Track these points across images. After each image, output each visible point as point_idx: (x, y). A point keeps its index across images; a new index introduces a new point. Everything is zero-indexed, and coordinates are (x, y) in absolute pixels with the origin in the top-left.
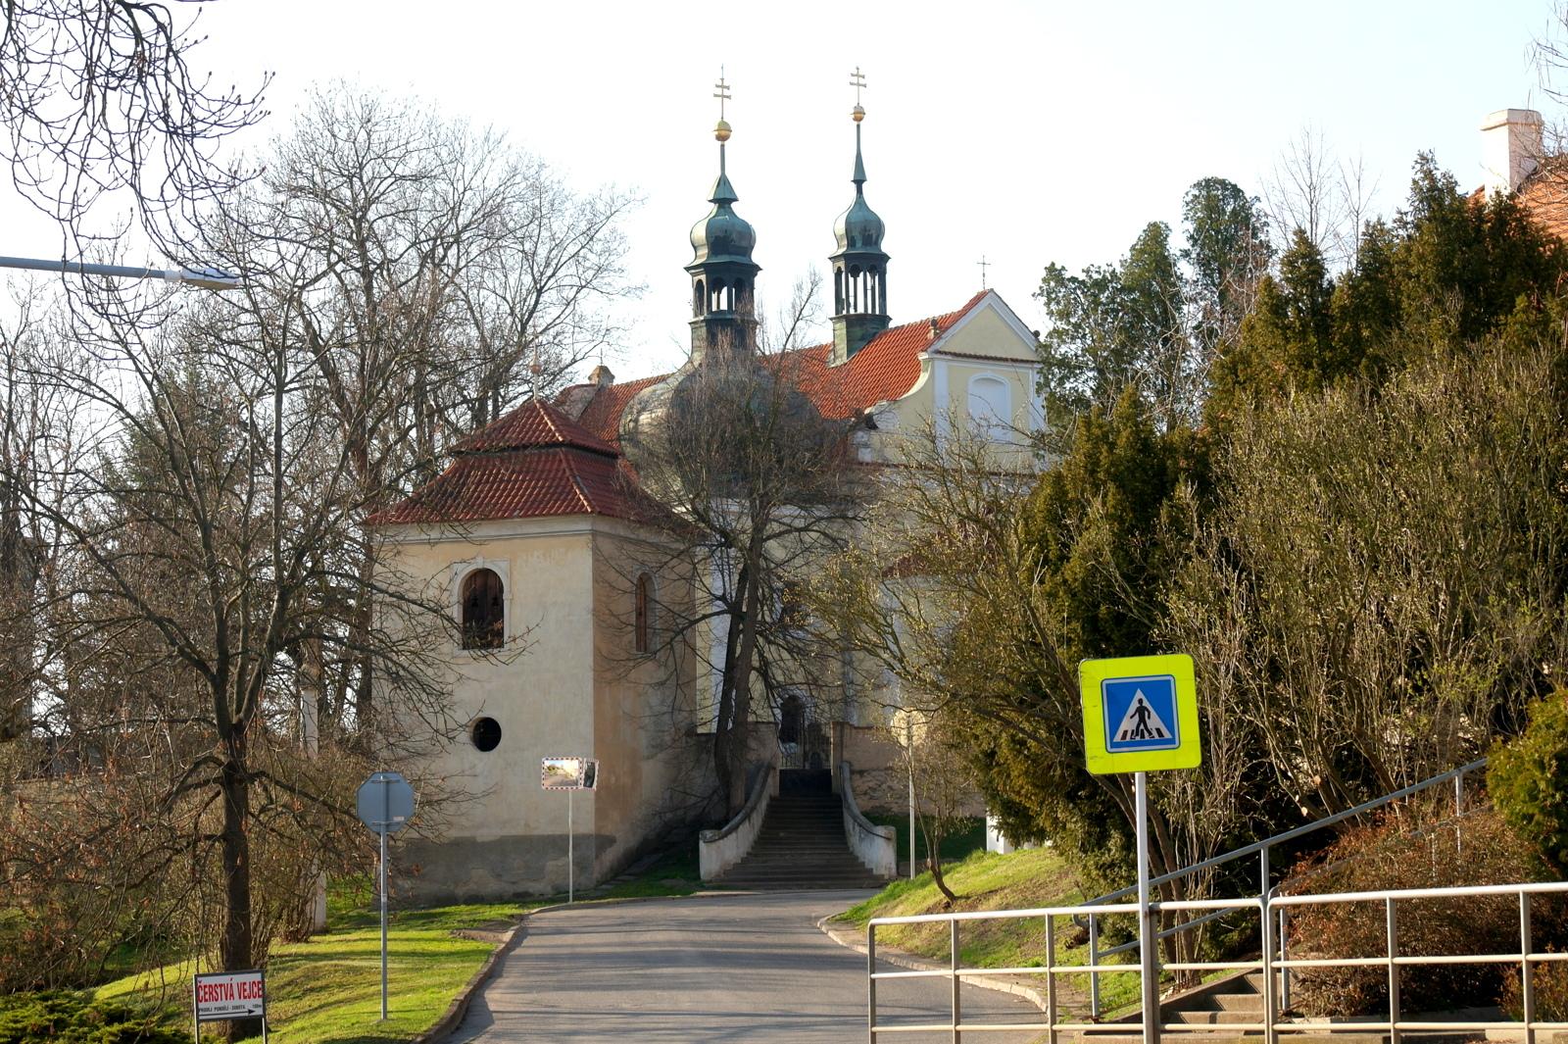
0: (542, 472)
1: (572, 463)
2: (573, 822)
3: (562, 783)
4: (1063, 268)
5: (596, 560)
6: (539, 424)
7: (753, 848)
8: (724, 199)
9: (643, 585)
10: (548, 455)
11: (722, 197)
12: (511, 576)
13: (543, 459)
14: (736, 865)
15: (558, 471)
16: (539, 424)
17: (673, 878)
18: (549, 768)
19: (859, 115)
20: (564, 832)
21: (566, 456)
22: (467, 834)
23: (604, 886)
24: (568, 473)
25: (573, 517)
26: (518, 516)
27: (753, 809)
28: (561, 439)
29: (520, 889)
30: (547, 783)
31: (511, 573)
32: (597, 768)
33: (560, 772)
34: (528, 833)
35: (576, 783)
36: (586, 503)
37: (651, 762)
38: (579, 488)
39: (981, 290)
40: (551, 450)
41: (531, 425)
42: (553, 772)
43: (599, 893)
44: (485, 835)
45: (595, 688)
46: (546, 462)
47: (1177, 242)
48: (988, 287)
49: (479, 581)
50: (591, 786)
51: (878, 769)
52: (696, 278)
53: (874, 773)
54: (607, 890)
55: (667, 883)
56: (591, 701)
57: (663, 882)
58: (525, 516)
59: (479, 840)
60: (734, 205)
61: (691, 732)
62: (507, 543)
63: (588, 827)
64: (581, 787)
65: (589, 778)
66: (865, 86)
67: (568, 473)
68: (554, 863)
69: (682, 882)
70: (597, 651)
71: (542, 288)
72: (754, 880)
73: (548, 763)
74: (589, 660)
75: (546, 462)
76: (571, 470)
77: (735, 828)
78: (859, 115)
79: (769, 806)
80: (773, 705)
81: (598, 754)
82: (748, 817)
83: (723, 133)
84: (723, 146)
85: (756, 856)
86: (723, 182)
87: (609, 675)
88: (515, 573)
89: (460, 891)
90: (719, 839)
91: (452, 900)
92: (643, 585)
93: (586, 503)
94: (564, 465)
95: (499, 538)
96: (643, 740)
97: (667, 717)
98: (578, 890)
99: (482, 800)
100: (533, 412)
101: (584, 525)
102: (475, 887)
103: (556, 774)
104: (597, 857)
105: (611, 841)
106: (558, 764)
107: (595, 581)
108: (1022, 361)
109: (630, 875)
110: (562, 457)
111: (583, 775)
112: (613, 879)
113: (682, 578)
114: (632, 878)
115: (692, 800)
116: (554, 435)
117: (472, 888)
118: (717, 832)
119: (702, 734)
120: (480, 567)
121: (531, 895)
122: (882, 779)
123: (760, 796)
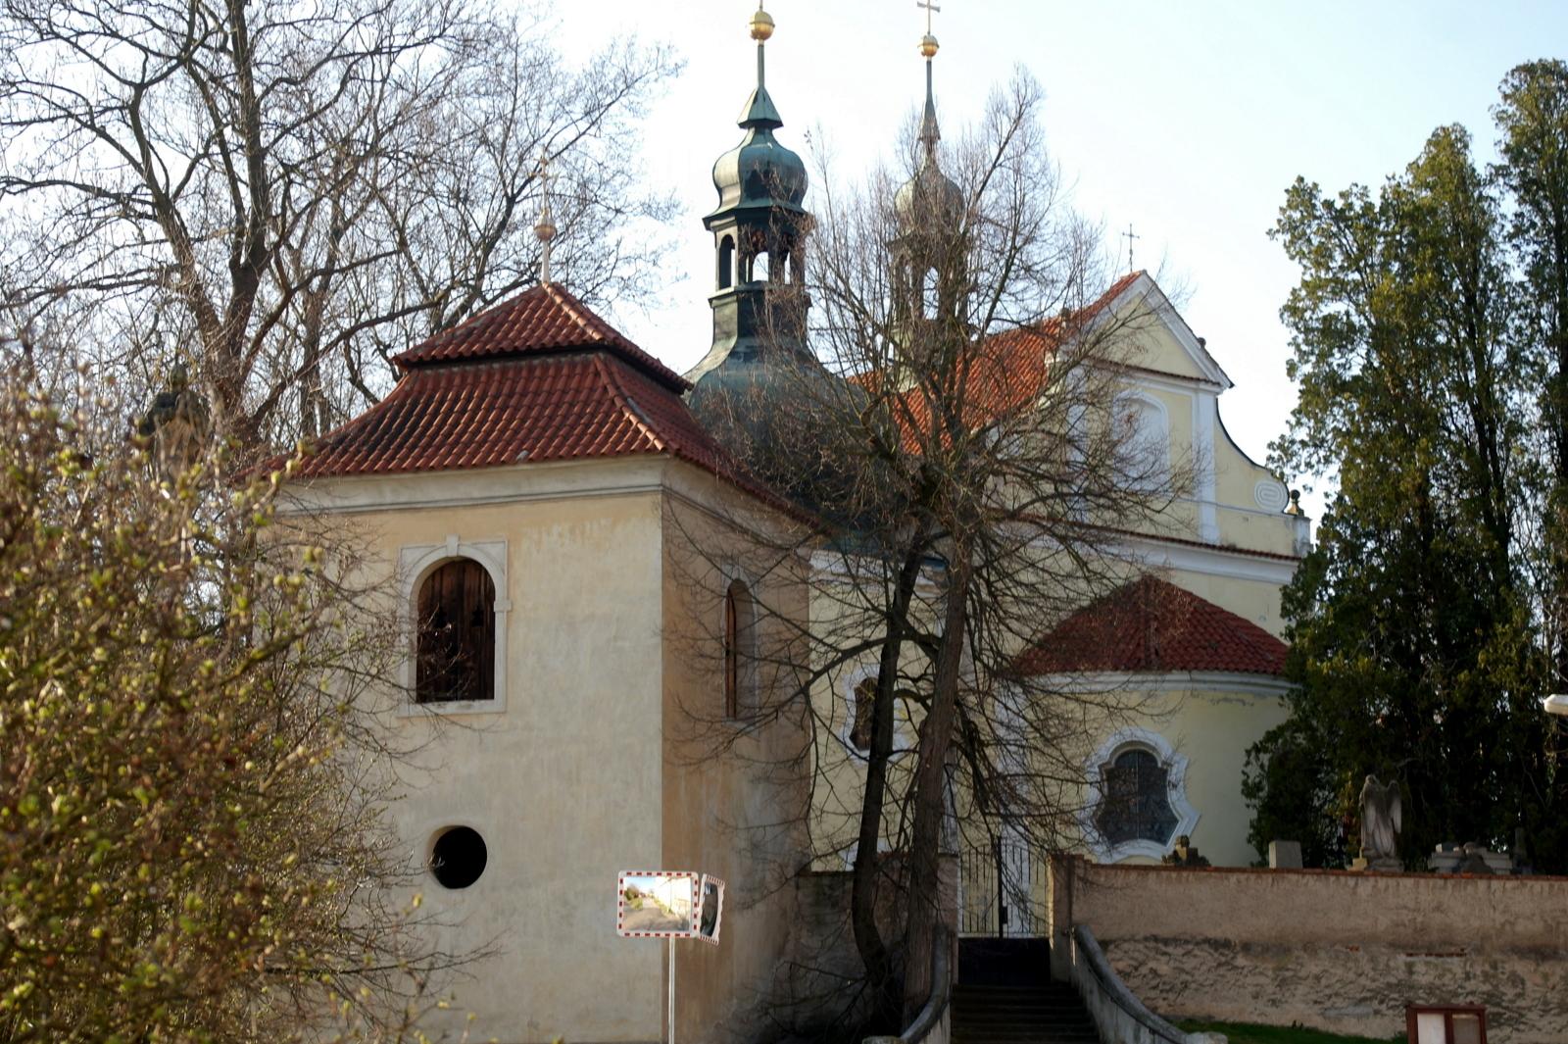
0: (564, 392)
3: (651, 926)
4: (1315, 185)
5: (667, 540)
6: (554, 319)
8: (763, 122)
10: (573, 366)
11: (761, 116)
12: (508, 568)
15: (592, 390)
16: (554, 319)
19: (930, 48)
24: (611, 392)
26: (531, 461)
28: (596, 336)
30: (628, 922)
33: (647, 903)
35: (684, 925)
36: (651, 437)
38: (634, 413)
39: (1126, 273)
42: (634, 903)
46: (569, 377)
47: (1485, 152)
48: (1136, 269)
49: (448, 582)
51: (1132, 939)
52: (721, 234)
53: (1126, 946)
56: (656, 796)
58: (542, 458)
60: (777, 133)
61: (803, 871)
66: (938, 10)
67: (611, 392)
71: (514, 196)
74: (655, 721)
75: (569, 377)
76: (618, 388)
78: (930, 48)
83: (763, 27)
84: (761, 47)
86: (761, 97)
88: (517, 564)
92: (736, 596)
93: (651, 437)
94: (604, 379)
95: (476, 504)
99: (470, 968)
100: (541, 300)
101: (648, 476)
103: (639, 908)
106: (643, 884)
107: (665, 576)
108: (1184, 378)
110: (600, 367)
116: (584, 332)
122: (1141, 958)
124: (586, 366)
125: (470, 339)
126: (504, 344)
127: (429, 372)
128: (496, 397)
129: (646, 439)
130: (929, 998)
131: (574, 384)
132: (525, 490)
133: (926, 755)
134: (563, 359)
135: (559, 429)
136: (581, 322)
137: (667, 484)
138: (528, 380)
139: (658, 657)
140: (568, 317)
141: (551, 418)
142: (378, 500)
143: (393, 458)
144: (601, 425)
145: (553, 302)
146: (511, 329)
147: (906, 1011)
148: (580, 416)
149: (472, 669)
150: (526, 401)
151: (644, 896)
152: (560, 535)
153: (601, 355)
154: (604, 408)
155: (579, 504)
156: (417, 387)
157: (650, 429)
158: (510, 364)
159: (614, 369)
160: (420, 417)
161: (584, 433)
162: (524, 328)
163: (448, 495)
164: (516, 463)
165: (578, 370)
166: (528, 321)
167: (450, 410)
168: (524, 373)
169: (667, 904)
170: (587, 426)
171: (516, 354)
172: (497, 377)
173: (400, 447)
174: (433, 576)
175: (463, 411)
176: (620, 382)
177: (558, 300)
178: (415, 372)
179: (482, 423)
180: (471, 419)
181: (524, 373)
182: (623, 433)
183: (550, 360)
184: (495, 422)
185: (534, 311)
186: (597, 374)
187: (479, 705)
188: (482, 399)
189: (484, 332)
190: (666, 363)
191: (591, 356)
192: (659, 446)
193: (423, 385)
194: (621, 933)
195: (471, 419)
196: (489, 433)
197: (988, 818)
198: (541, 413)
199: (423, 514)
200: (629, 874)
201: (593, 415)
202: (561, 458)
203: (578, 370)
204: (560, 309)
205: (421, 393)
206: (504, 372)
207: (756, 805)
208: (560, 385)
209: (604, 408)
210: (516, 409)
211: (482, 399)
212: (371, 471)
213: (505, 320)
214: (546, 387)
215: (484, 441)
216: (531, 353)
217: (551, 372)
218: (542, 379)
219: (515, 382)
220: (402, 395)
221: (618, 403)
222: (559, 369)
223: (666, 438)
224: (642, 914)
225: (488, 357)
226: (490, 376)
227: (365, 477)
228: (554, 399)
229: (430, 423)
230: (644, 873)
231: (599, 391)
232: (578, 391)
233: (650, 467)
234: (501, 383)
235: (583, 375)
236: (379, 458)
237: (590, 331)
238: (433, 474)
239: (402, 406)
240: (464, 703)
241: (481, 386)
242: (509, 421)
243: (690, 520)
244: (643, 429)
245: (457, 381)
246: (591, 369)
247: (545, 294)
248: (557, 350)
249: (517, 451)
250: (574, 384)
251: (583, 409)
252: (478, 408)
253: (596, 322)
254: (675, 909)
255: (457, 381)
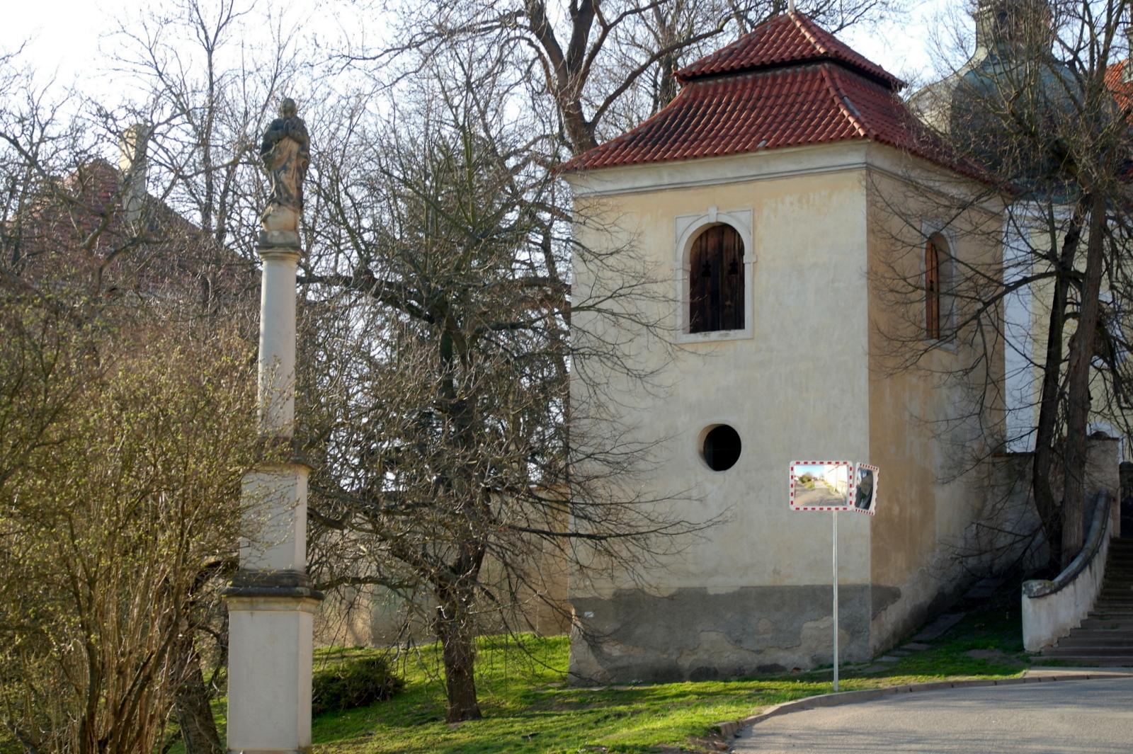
0: (798, 95)
1: (839, 84)
2: (840, 569)
3: (822, 502)
5: (871, 203)
6: (794, 39)
7: (1095, 606)
9: (935, 245)
10: (805, 74)
12: (753, 230)
13: (799, 79)
14: (1074, 630)
15: (818, 92)
16: (794, 39)
17: (985, 648)
18: (801, 479)
20: (815, 579)
21: (829, 72)
22: (694, 583)
23: (884, 659)
24: (832, 92)
25: (839, 146)
26: (767, 148)
27: (1095, 552)
28: (822, 51)
29: (768, 660)
30: (799, 502)
31: (754, 227)
32: (876, 479)
33: (818, 485)
34: (778, 583)
35: (843, 502)
36: (856, 126)
37: (947, 487)
38: (847, 108)
40: (810, 68)
41: (784, 40)
42: (808, 485)
43: (876, 669)
44: (720, 585)
45: (872, 381)
46: (802, 83)
49: (712, 241)
50: (867, 506)
54: (888, 664)
55: (977, 655)
56: (864, 399)
57: (971, 653)
58: (776, 146)
59: (711, 592)
61: (998, 451)
62: (750, 186)
63: (861, 574)
64: (853, 507)
65: (864, 497)
67: (832, 92)
68: (811, 624)
69: (997, 655)
70: (874, 327)
72: (1104, 653)
73: (799, 471)
74: (862, 342)
75: (802, 83)
76: (837, 90)
77: (1074, 577)
79: (1110, 549)
80: (1124, 405)
81: (877, 455)
82: (1088, 562)
85: (1101, 617)
87: (890, 363)
89: (686, 662)
90: (1052, 592)
91: (674, 675)
92: (935, 245)
93: (856, 126)
94: (828, 84)
95: (736, 181)
96: (937, 458)
97: (974, 421)
98: (847, 664)
100: (786, 25)
101: (855, 156)
102: (706, 657)
103: (812, 489)
104: (874, 617)
105: (894, 595)
106: (816, 471)
107: (871, 231)
109: (920, 642)
110: (825, 73)
111: (854, 490)
112: (897, 647)
113: (1079, 49)
114: (923, 647)
115: (1003, 541)
117: (701, 657)
118: (1047, 583)
119: (1015, 454)
120: (713, 219)
121: (782, 669)
123: (1101, 536)
124: (815, 73)
125: (731, 58)
126: (755, 60)
127: (701, 84)
128: (748, 101)
129: (854, 128)
130: (1081, 550)
131: (805, 88)
132: (765, 170)
133: (1074, 363)
134: (798, 70)
135: (791, 123)
136: (812, 40)
137: (869, 161)
138: (772, 86)
139: (864, 294)
140: (804, 37)
141: (786, 115)
142: (659, 182)
143: (668, 150)
144: (822, 119)
145: (794, 26)
146: (761, 48)
147: (1064, 559)
148: (807, 112)
149: (730, 306)
150: (769, 103)
151: (816, 479)
152: (792, 204)
153: (826, 65)
154: (826, 106)
155: (805, 179)
156: (691, 96)
157: (857, 120)
158: (760, 75)
159: (836, 75)
160: (692, 118)
161: (809, 125)
162: (771, 47)
163: (709, 176)
164: (757, 150)
165: (809, 77)
166: (774, 42)
167: (714, 112)
168: (769, 81)
169: (834, 485)
170: (812, 120)
171: (763, 67)
172: (749, 85)
173: (675, 141)
174: (701, 237)
175: (724, 112)
176: (839, 84)
177: (798, 24)
178: (691, 84)
179: (736, 121)
180: (729, 118)
181: (769, 81)
182: (838, 124)
183: (789, 71)
184: (746, 120)
185: (780, 33)
186: (823, 80)
187: (734, 333)
188: (738, 102)
189: (741, 52)
190: (886, 68)
191: (819, 66)
192: (862, 133)
193: (697, 93)
194: (793, 508)
195: (729, 118)
196: (740, 128)
197: (1125, 412)
198: (779, 112)
199: (691, 191)
200: (798, 463)
201: (817, 111)
202: (789, 145)
203: (809, 77)
204: (799, 31)
205: (694, 100)
206: (755, 81)
207: (953, 400)
208: (795, 90)
209: (826, 106)
210: (762, 109)
211: (738, 102)
212: (653, 161)
213: (758, 41)
214: (785, 91)
215: (736, 134)
216: (774, 66)
217: (789, 80)
218: (782, 86)
219: (762, 88)
220: (681, 101)
221: (837, 100)
222: (795, 78)
223: (868, 126)
224: (815, 492)
225: (743, 70)
226: (745, 84)
227: (647, 165)
228: (790, 100)
229: (698, 123)
230: (818, 462)
231: (823, 92)
232: (808, 93)
233: (856, 150)
234: (752, 90)
235: (813, 81)
236: (658, 151)
237: (818, 47)
238: (697, 161)
239: (680, 110)
240: (723, 332)
241: (738, 92)
242: (756, 119)
243: (886, 186)
244: (851, 120)
245: (720, 90)
246: (819, 76)
247: (790, 20)
248: (793, 63)
249: (760, 140)
250: (805, 88)
251: (810, 107)
252: (734, 109)
253: (828, 38)
254: (839, 489)
255: (720, 90)
